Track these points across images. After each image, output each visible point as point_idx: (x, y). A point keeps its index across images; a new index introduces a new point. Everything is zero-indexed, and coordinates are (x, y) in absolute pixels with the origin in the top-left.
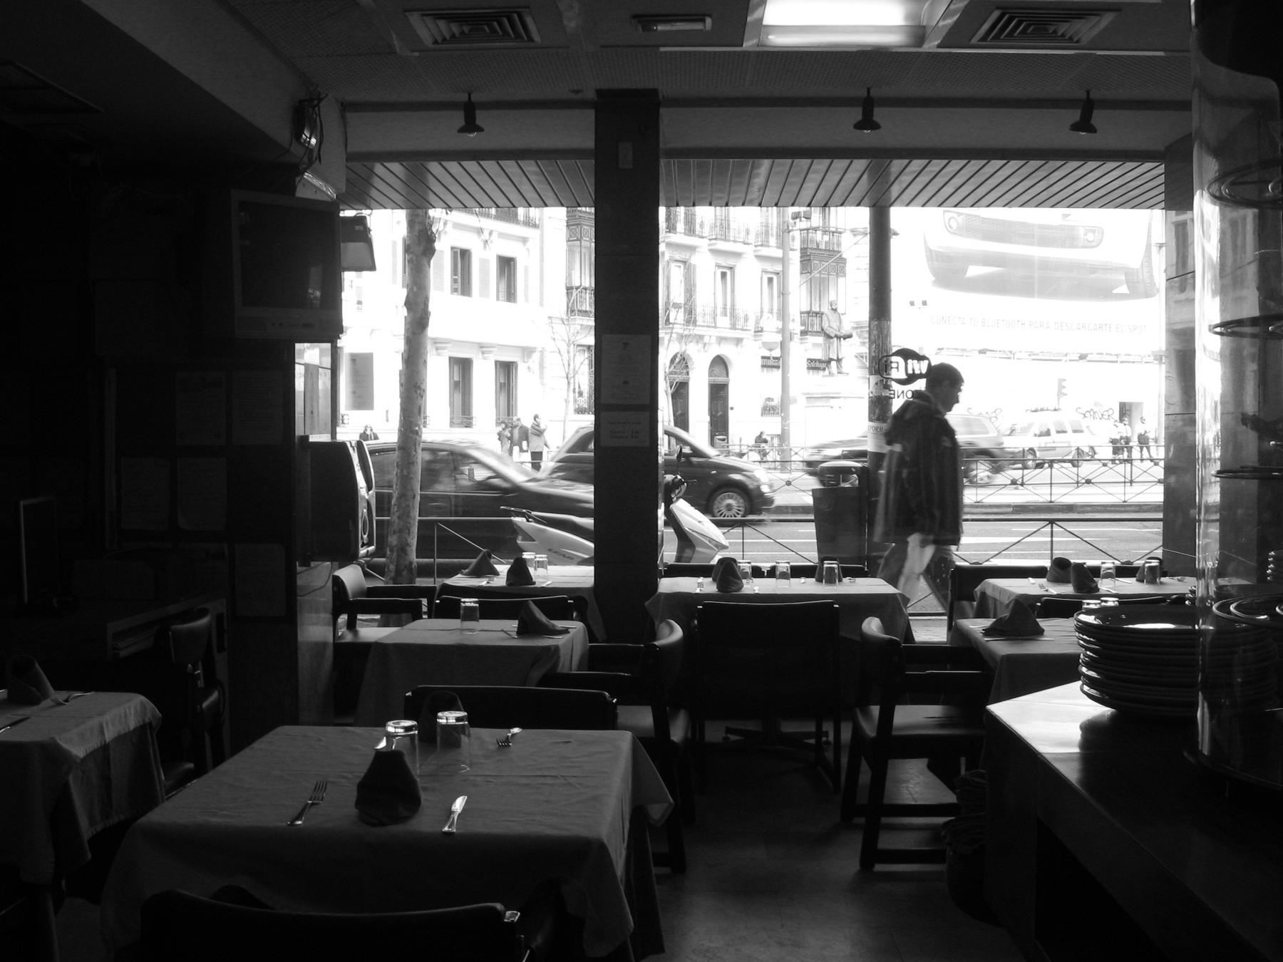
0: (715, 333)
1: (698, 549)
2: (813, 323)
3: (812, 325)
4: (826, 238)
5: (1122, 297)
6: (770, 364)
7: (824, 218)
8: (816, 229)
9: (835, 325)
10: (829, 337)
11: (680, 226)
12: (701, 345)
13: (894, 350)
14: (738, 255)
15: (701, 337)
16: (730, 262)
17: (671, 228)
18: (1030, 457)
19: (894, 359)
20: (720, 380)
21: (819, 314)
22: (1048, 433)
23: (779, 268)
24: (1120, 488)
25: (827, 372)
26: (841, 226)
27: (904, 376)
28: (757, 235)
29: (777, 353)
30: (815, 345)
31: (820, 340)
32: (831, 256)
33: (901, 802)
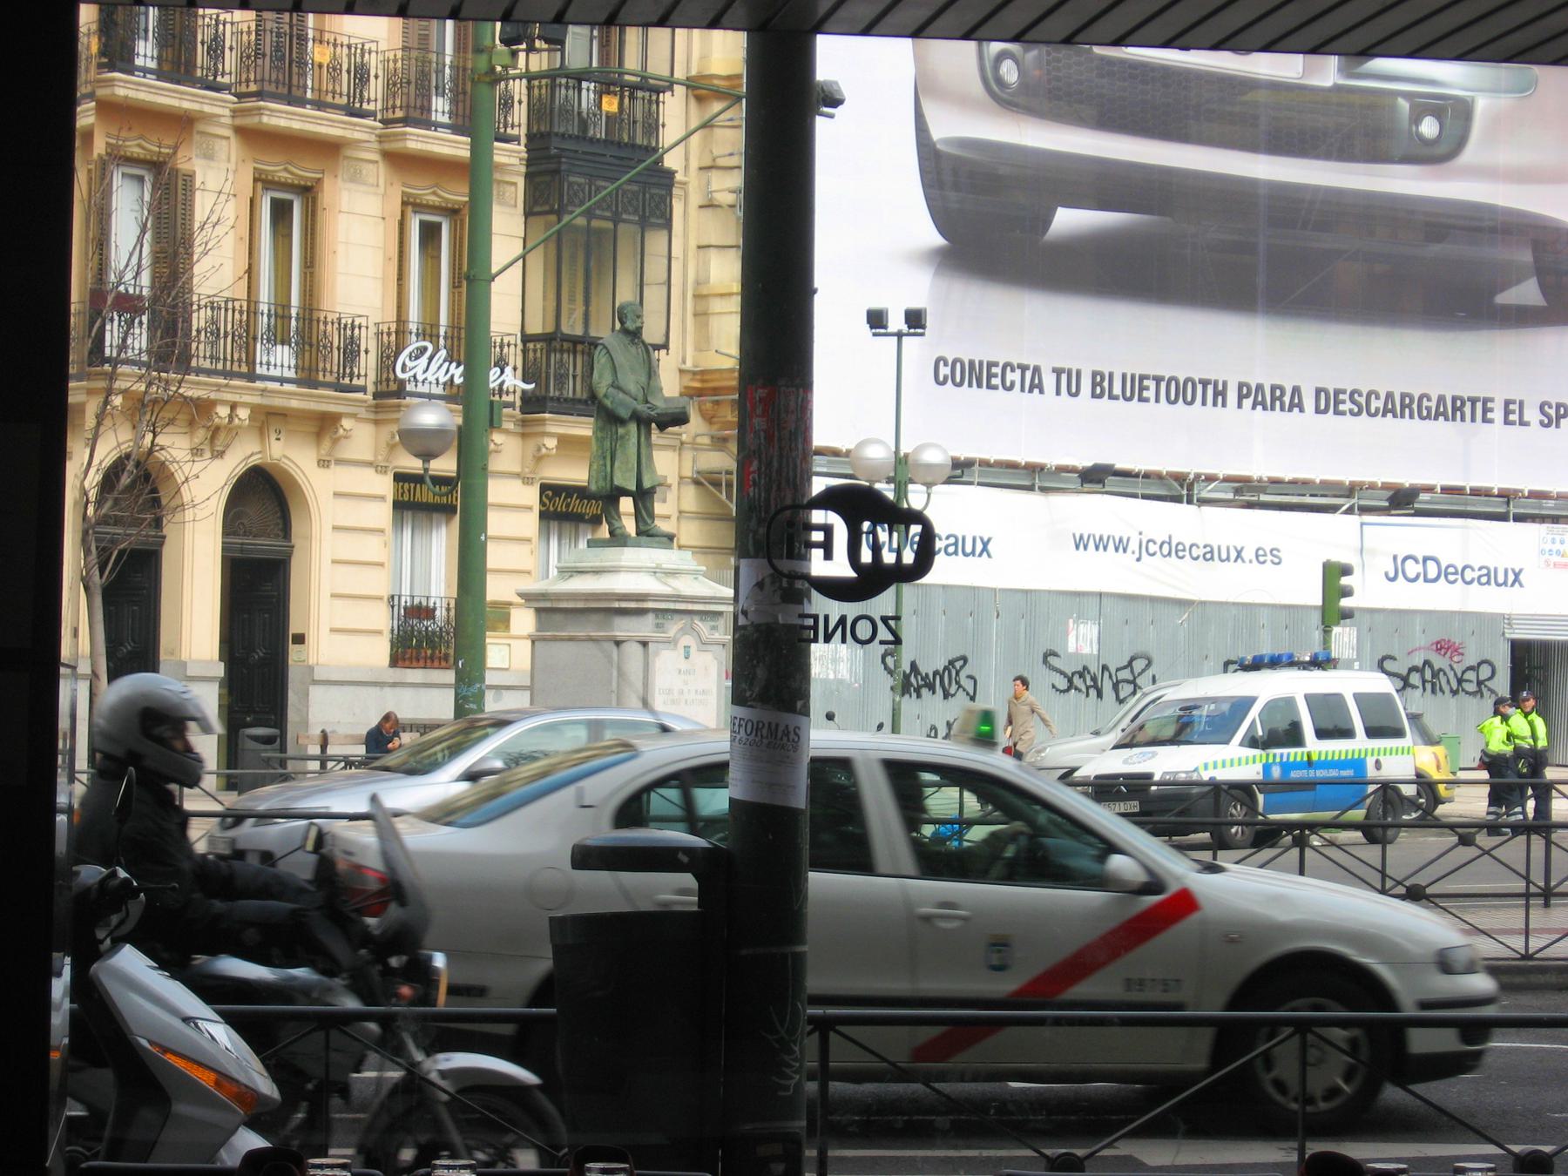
0: (247, 396)
1: (180, 1108)
2: (573, 372)
3: (561, 379)
4: (610, 105)
5: (1522, 318)
6: (418, 501)
7: (605, 45)
8: (579, 77)
9: (632, 382)
10: (610, 419)
11: (146, 52)
12: (201, 434)
13: (818, 485)
14: (329, 149)
15: (203, 408)
16: (303, 171)
17: (118, 56)
18: (1237, 812)
19: (818, 516)
20: (264, 545)
21: (585, 345)
22: (1293, 736)
23: (457, 194)
24: (1512, 917)
25: (604, 532)
26: (658, 67)
27: (847, 572)
28: (391, 86)
29: (445, 465)
30: (565, 442)
31: (583, 428)
32: (624, 164)
33: (69, 444)
